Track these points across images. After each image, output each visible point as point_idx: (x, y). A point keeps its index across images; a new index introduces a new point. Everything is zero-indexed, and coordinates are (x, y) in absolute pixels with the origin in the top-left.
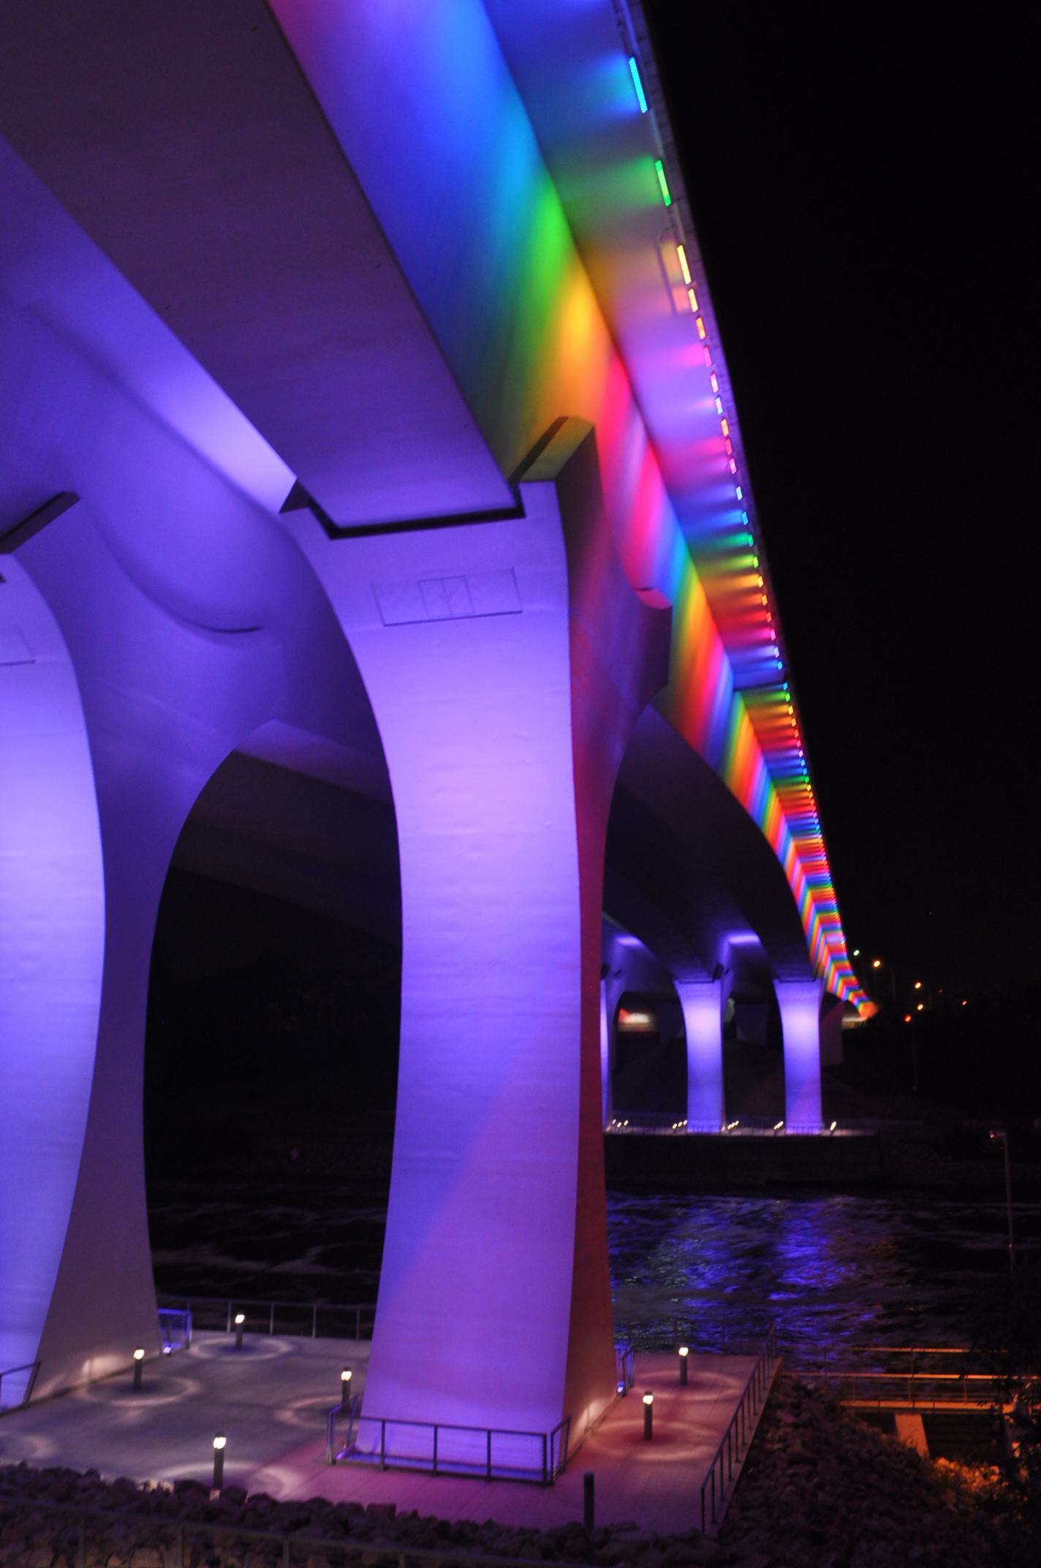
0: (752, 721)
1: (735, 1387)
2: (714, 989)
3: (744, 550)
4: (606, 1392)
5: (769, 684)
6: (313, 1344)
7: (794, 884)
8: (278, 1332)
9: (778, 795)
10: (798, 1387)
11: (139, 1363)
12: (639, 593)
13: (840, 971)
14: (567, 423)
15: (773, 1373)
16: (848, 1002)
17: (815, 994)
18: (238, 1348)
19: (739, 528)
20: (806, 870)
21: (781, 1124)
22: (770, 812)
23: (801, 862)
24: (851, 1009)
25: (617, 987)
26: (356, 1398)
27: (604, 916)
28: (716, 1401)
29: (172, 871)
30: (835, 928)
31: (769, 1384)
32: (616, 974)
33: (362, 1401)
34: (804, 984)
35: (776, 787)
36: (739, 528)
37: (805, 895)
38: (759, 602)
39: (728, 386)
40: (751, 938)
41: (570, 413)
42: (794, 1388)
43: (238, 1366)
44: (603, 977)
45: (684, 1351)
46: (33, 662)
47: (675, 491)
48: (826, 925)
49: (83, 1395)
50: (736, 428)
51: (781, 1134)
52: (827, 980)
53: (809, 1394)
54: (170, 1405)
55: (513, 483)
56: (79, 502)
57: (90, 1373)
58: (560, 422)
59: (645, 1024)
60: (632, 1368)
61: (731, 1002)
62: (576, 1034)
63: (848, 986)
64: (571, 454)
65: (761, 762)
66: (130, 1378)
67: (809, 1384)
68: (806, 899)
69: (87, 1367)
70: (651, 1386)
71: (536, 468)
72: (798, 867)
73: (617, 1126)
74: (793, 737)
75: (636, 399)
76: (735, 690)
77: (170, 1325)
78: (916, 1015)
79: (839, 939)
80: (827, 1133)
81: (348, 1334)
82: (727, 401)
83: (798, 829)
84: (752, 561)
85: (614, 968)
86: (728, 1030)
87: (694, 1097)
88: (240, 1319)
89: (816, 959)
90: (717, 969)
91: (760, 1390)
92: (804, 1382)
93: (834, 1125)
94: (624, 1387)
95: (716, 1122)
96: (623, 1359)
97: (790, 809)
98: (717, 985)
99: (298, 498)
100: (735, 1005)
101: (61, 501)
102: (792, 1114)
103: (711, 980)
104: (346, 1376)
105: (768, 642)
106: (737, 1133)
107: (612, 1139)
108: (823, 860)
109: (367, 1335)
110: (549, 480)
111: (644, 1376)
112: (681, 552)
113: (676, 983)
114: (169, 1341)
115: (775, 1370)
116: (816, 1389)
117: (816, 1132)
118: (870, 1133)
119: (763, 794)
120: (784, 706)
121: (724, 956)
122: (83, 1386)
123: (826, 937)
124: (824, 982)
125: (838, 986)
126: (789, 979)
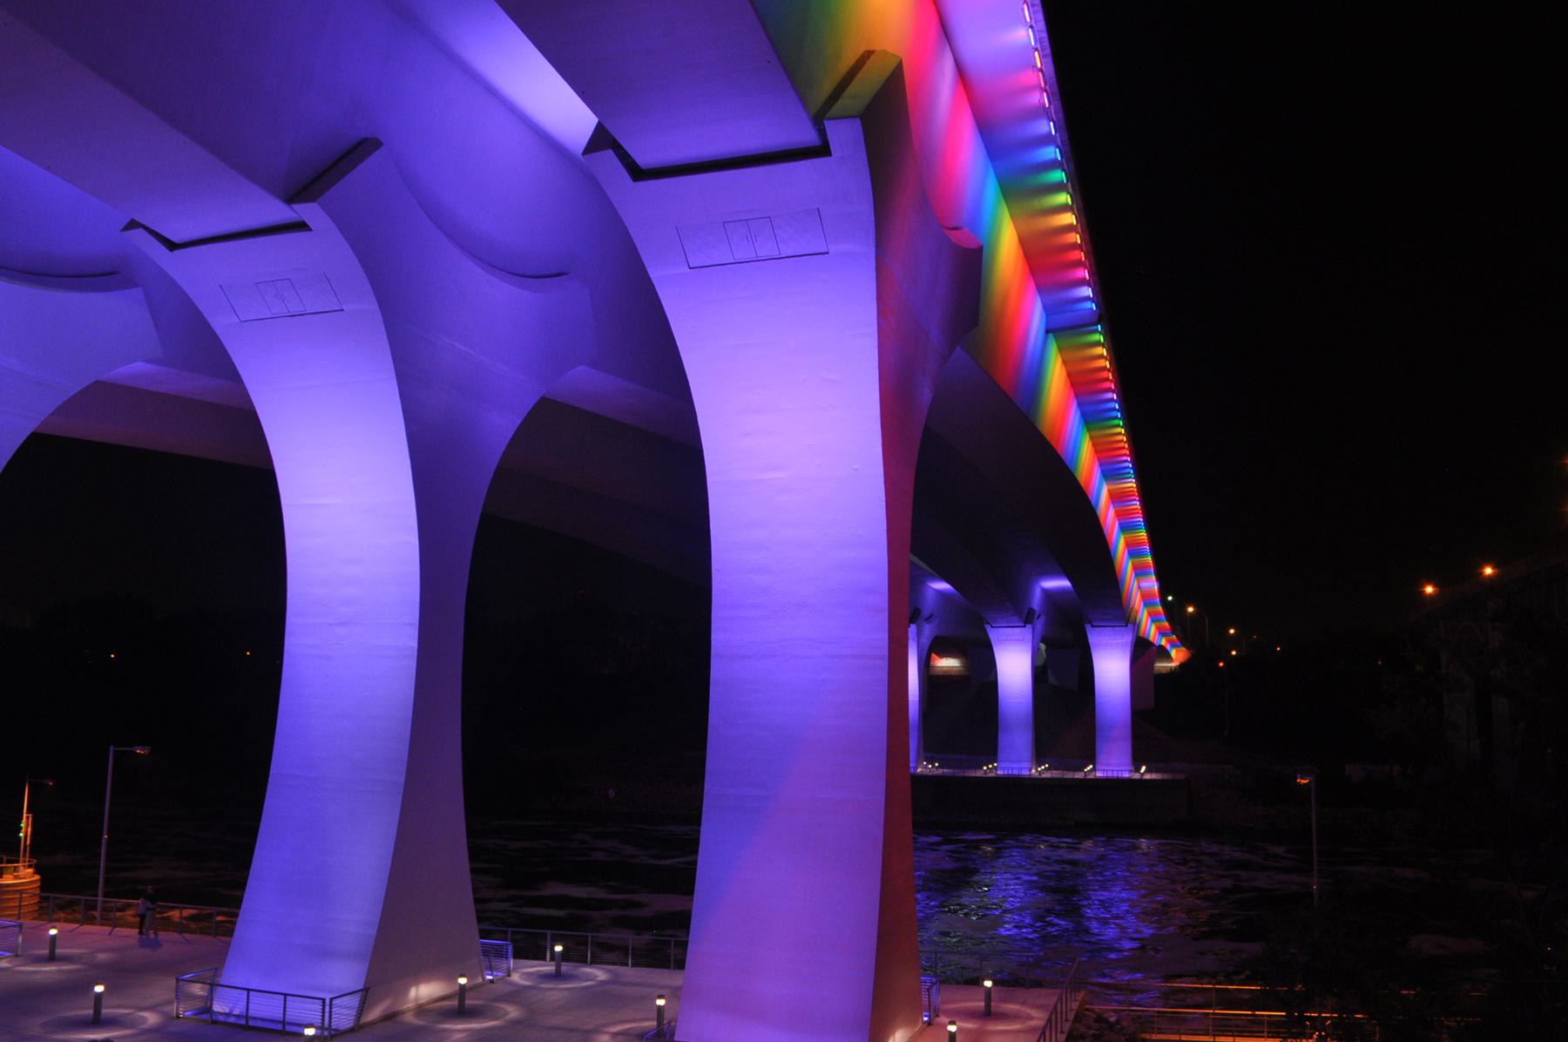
0: (1064, 362)
1: (1038, 1018)
2: (1026, 633)
3: (1057, 187)
4: (910, 1022)
5: (1081, 326)
6: (629, 973)
7: (1107, 530)
8: (595, 962)
9: (1091, 438)
10: (1100, 1019)
11: (462, 987)
12: (946, 232)
13: (1153, 617)
14: (873, 58)
15: (1075, 1005)
16: (1162, 647)
17: (1128, 639)
18: (557, 976)
19: (1051, 165)
20: (1118, 515)
21: (1091, 766)
22: (1084, 457)
23: (1114, 507)
24: (1164, 654)
25: (929, 630)
26: (669, 1023)
27: (915, 559)
28: (1018, 1031)
29: (485, 519)
30: (1147, 574)
31: (1071, 1016)
32: (928, 619)
33: (675, 1026)
35: (1089, 430)
36: (1051, 165)
38: (1074, 240)
39: (1041, 16)
40: (1065, 583)
41: (877, 46)
42: (1096, 1021)
43: (557, 993)
44: (911, 621)
45: (988, 984)
46: (342, 310)
47: (986, 127)
48: (1139, 571)
49: (409, 1018)
50: (1049, 60)
51: (1091, 776)
52: (1139, 625)
53: (1111, 1026)
54: (493, 1028)
55: (818, 121)
56: (382, 148)
57: (417, 999)
58: (868, 54)
60: (937, 999)
61: (1043, 646)
62: (883, 676)
64: (878, 88)
66: (455, 1003)
67: (1111, 1016)
68: (1120, 545)
69: (413, 992)
70: (954, 1017)
71: (845, 103)
72: (1112, 512)
73: (924, 768)
74: (1107, 379)
75: (945, 31)
76: (1048, 331)
77: (492, 955)
78: (1230, 661)
79: (1152, 584)
80: (1136, 776)
81: (663, 963)
82: (1040, 31)
83: (1111, 473)
84: (1064, 198)
85: (926, 613)
86: (1039, 674)
87: (1004, 740)
88: (558, 948)
89: (1129, 604)
90: (1029, 612)
91: (1062, 1023)
92: (1106, 1015)
93: (1143, 769)
94: (929, 1017)
95: (1027, 765)
96: (928, 990)
97: (1103, 453)
98: (1029, 628)
99: (601, 140)
100: (1046, 650)
101: (365, 147)
102: (1101, 757)
103: (1022, 625)
104: (661, 1002)
105: (1082, 282)
106: (1047, 775)
107: (918, 780)
108: (1137, 505)
109: (680, 965)
110: (854, 117)
111: (947, 1007)
112: (992, 190)
113: (987, 627)
114: (491, 969)
115: (1078, 1003)
116: (1118, 1022)
117: (1126, 775)
118: (1181, 777)
119: (1075, 441)
120: (1097, 349)
121: (1036, 601)
122: (409, 1010)
123: (1138, 583)
125: (1152, 632)
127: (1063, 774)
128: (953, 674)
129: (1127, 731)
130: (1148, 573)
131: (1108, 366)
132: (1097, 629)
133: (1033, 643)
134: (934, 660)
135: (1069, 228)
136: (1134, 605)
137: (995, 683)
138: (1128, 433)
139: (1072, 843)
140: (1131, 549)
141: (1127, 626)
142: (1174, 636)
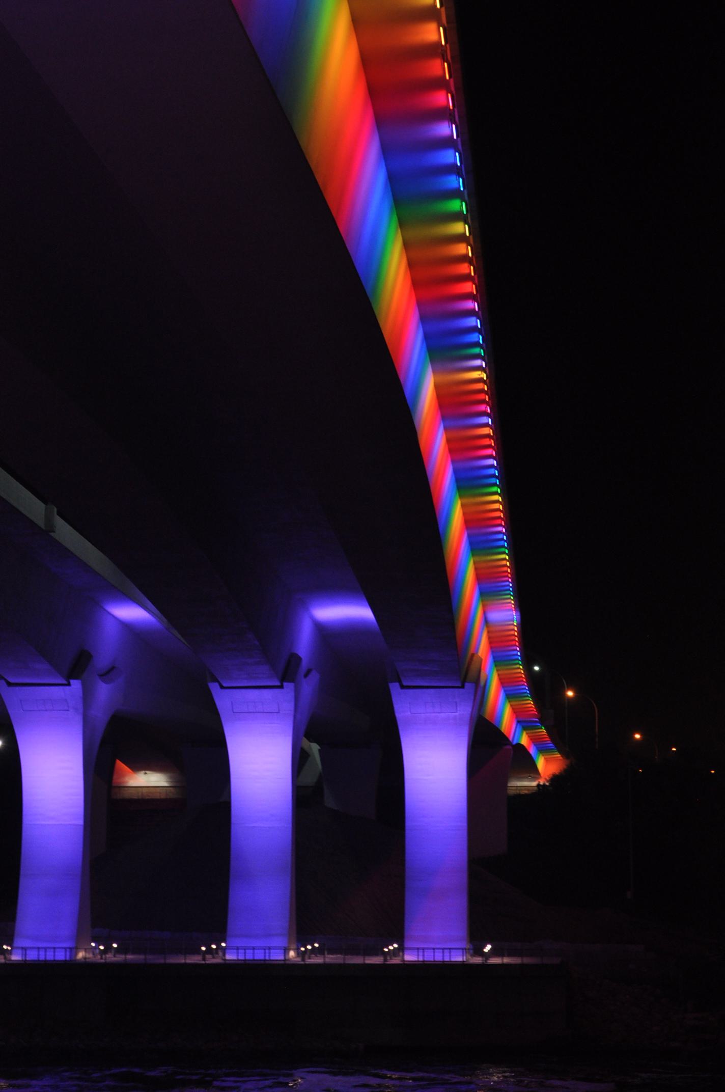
3: (454, 194)
13: (508, 686)
17: (464, 711)
37: (476, 609)
51: (396, 961)
63: (522, 721)
65: (441, 430)
80: (478, 960)
84: (458, 205)
95: (280, 942)
98: (289, 687)
102: (414, 928)
103: (65, 682)
106: (318, 960)
113: (214, 687)
117: (458, 958)
123: (484, 613)
127: (344, 959)
128: (157, 796)
129: (462, 879)
130: (503, 589)
131: (495, 465)
132: (411, 691)
133: (295, 717)
135: (433, 50)
136: (477, 649)
138: (495, 427)
140: (500, 672)
141: (463, 687)
142: (543, 730)
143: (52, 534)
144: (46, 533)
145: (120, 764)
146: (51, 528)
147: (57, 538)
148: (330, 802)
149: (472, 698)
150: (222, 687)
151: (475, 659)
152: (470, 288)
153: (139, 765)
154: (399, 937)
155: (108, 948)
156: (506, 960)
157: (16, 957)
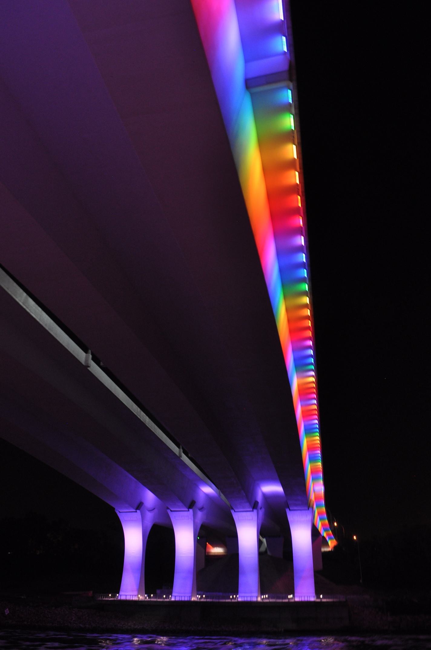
21: (292, 595)
34: (303, 511)
51: (293, 601)
59: (222, 553)
80: (319, 600)
87: (242, 580)
93: (321, 596)
95: (255, 594)
98: (255, 511)
102: (298, 590)
106: (267, 601)
117: (313, 599)
124: (313, 512)
126: (296, 508)
128: (220, 554)
129: (312, 573)
134: (210, 549)
137: (237, 555)
139: (285, 27)
141: (309, 509)
143: (181, 458)
144: (179, 458)
145: (209, 545)
146: (181, 456)
147: (183, 460)
148: (269, 553)
149: (311, 513)
150: (171, 511)
151: (312, 501)
152: (310, 334)
153: (215, 545)
154: (293, 593)
155: (202, 597)
156: (328, 600)
157: (173, 599)
